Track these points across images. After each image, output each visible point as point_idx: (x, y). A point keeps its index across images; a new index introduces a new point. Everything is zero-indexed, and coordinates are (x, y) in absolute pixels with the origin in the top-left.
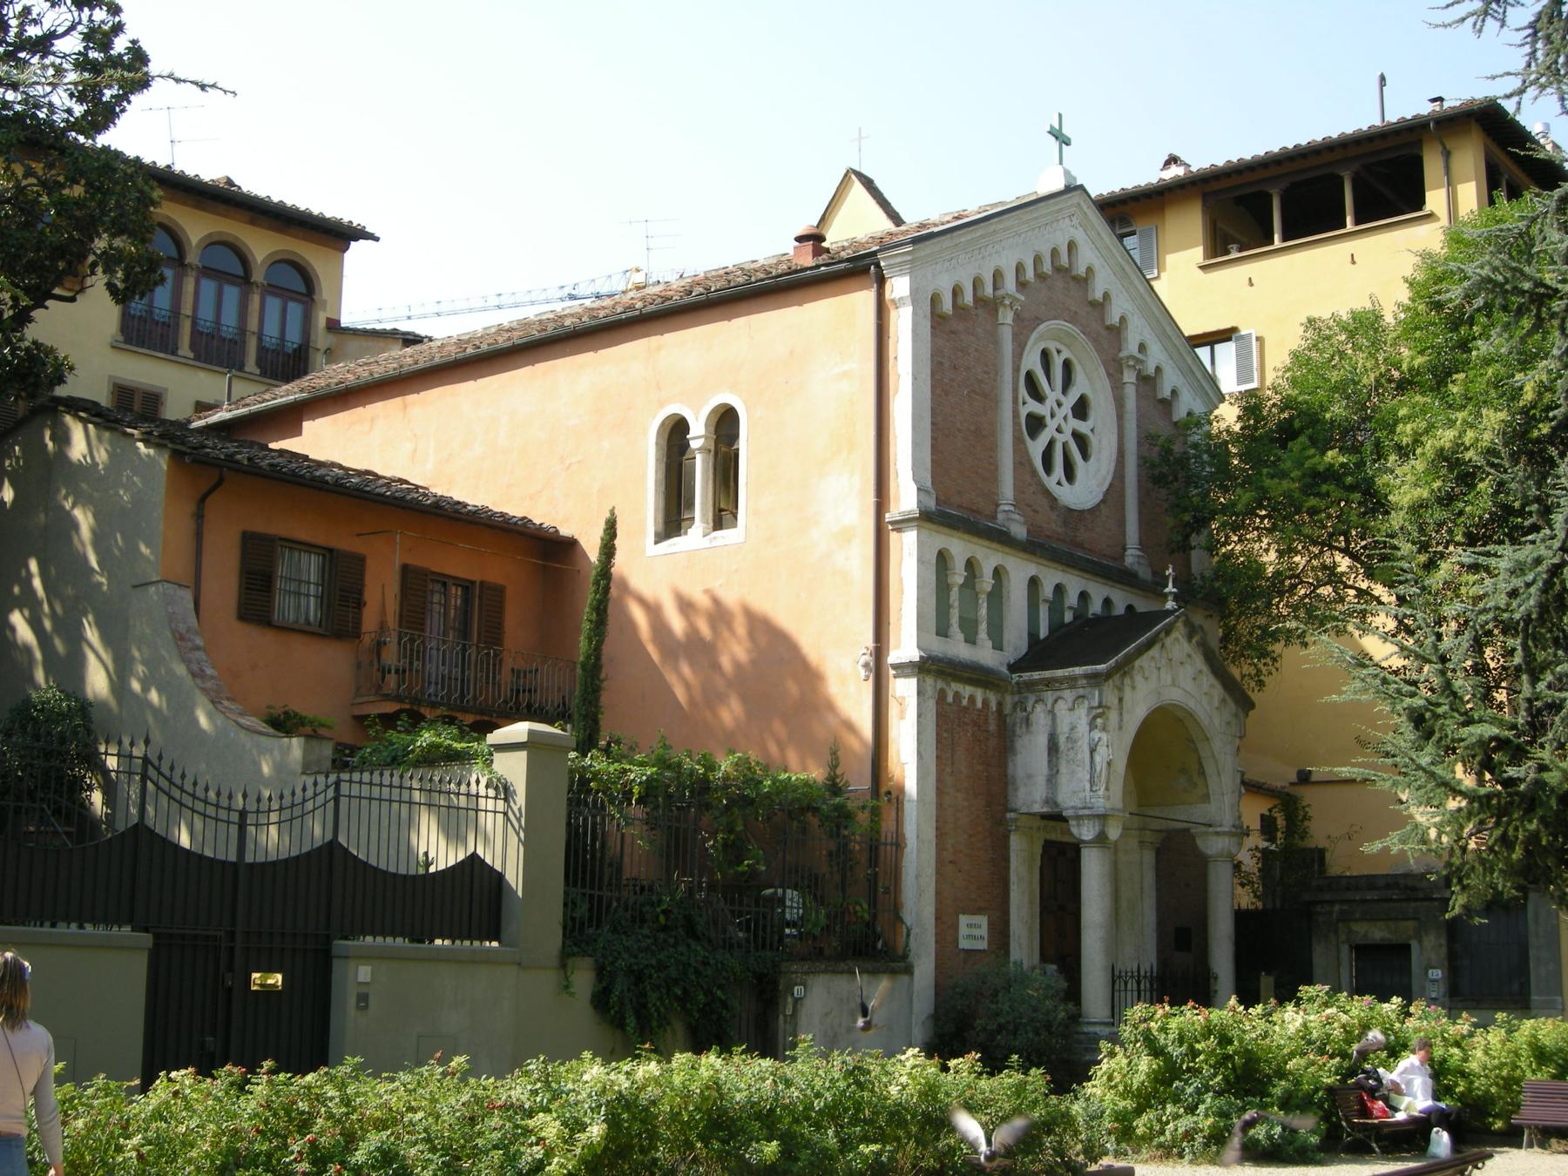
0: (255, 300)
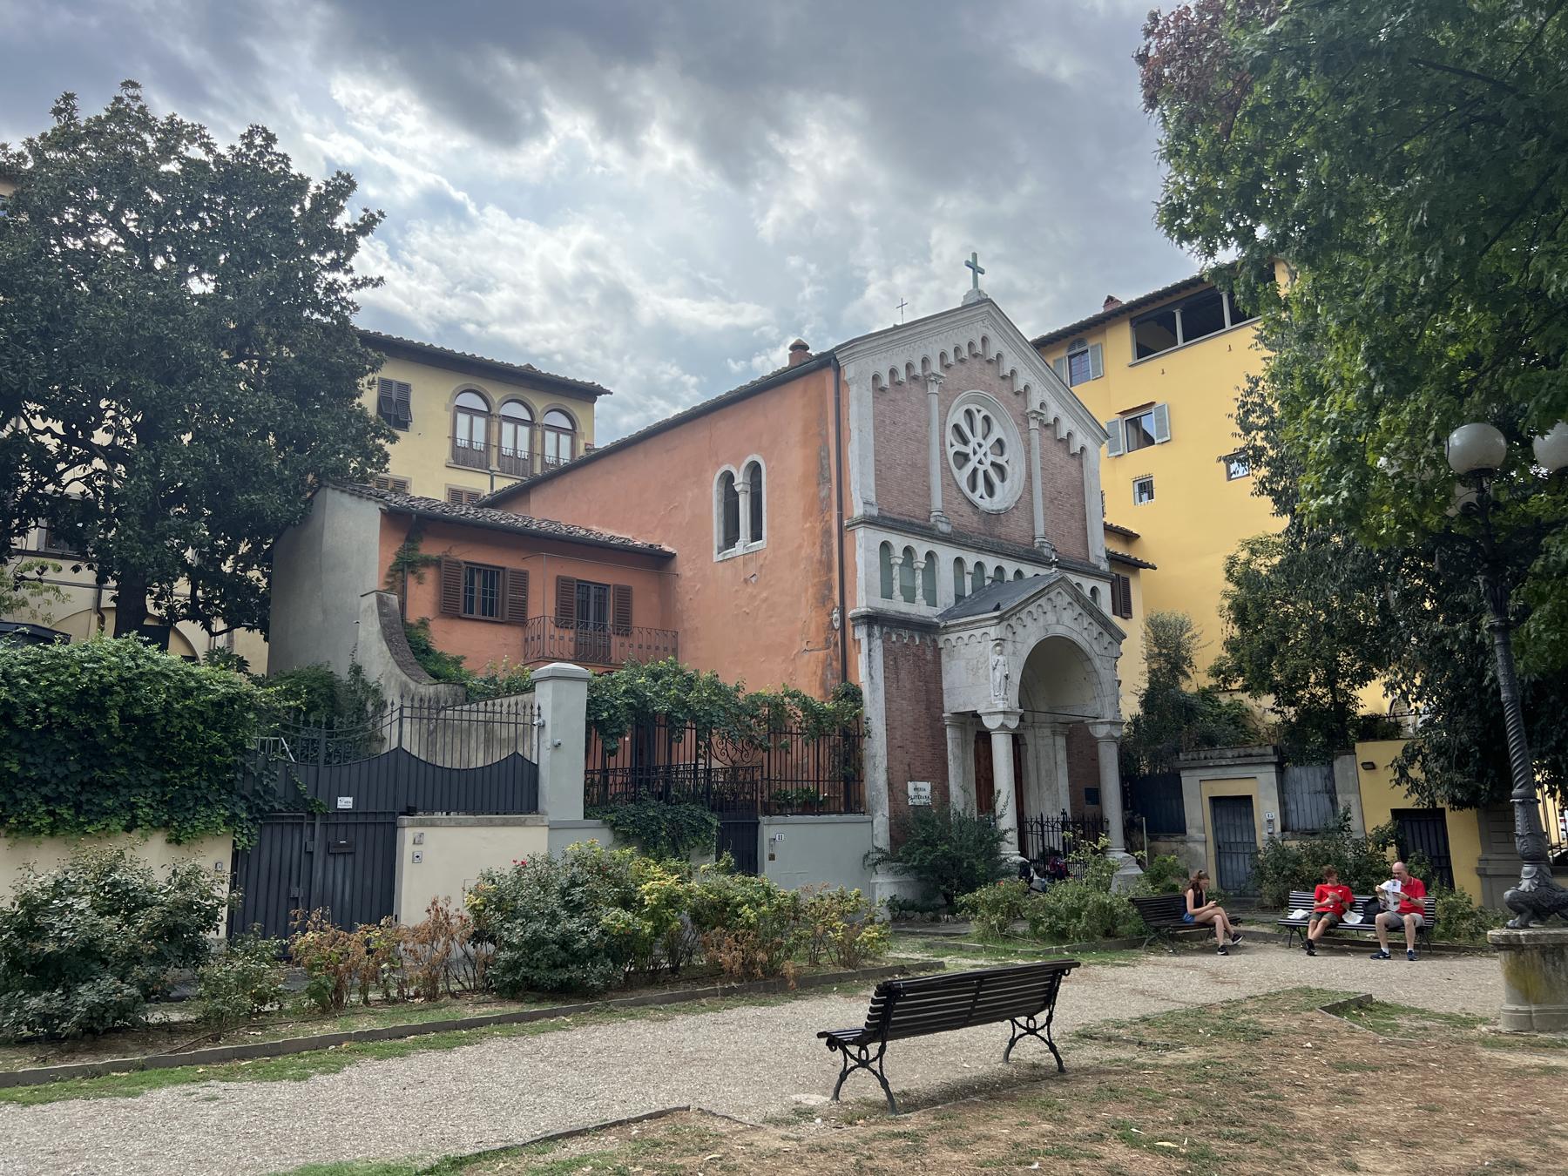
0: (539, 435)
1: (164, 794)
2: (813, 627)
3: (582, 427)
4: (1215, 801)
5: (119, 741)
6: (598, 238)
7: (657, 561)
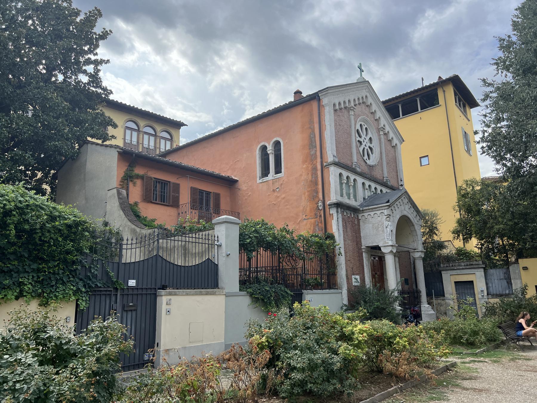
1: (39, 277)
2: (308, 209)
3: (175, 138)
4: (455, 282)
5: (13, 244)
6: (151, 89)
7: (230, 183)
